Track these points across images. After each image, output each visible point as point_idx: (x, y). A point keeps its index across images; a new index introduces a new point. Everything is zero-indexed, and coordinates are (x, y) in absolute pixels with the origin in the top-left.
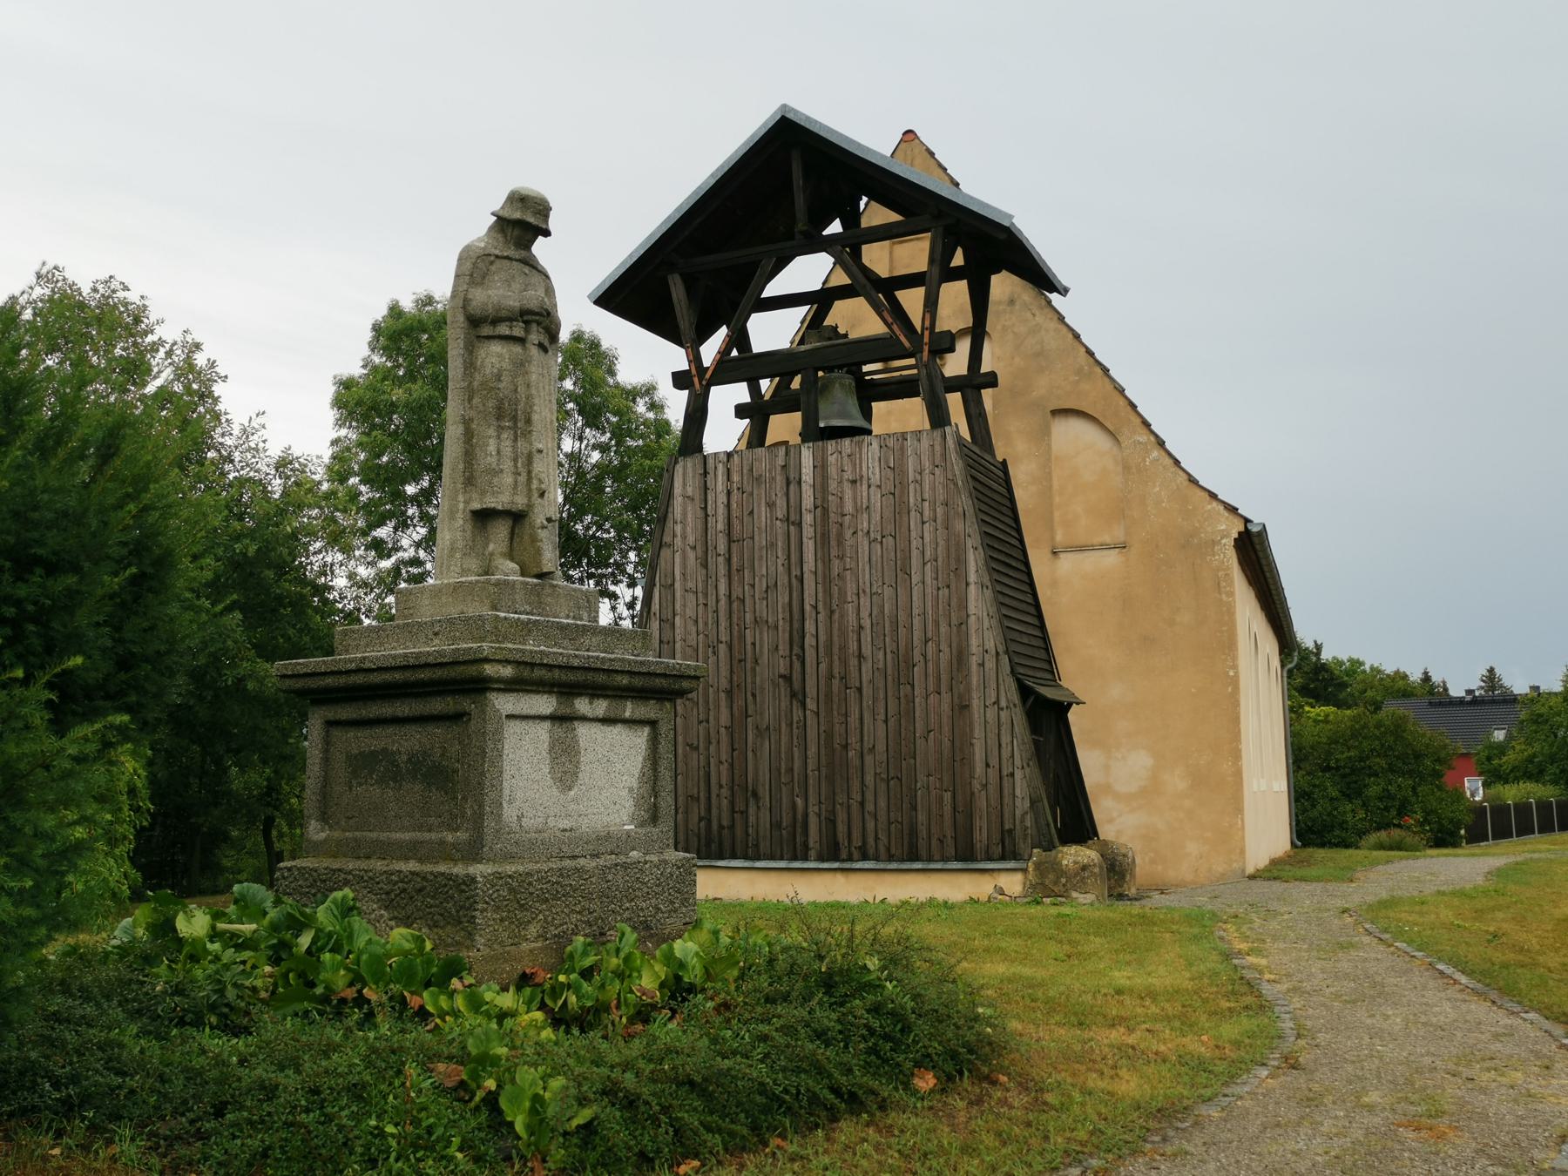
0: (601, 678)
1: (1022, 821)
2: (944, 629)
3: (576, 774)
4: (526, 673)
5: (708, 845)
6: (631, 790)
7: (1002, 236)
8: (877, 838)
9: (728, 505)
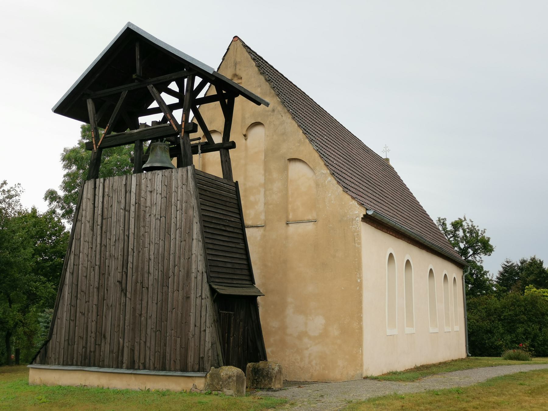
1: (208, 353)
5: (85, 360)
8: (150, 359)
9: (103, 202)
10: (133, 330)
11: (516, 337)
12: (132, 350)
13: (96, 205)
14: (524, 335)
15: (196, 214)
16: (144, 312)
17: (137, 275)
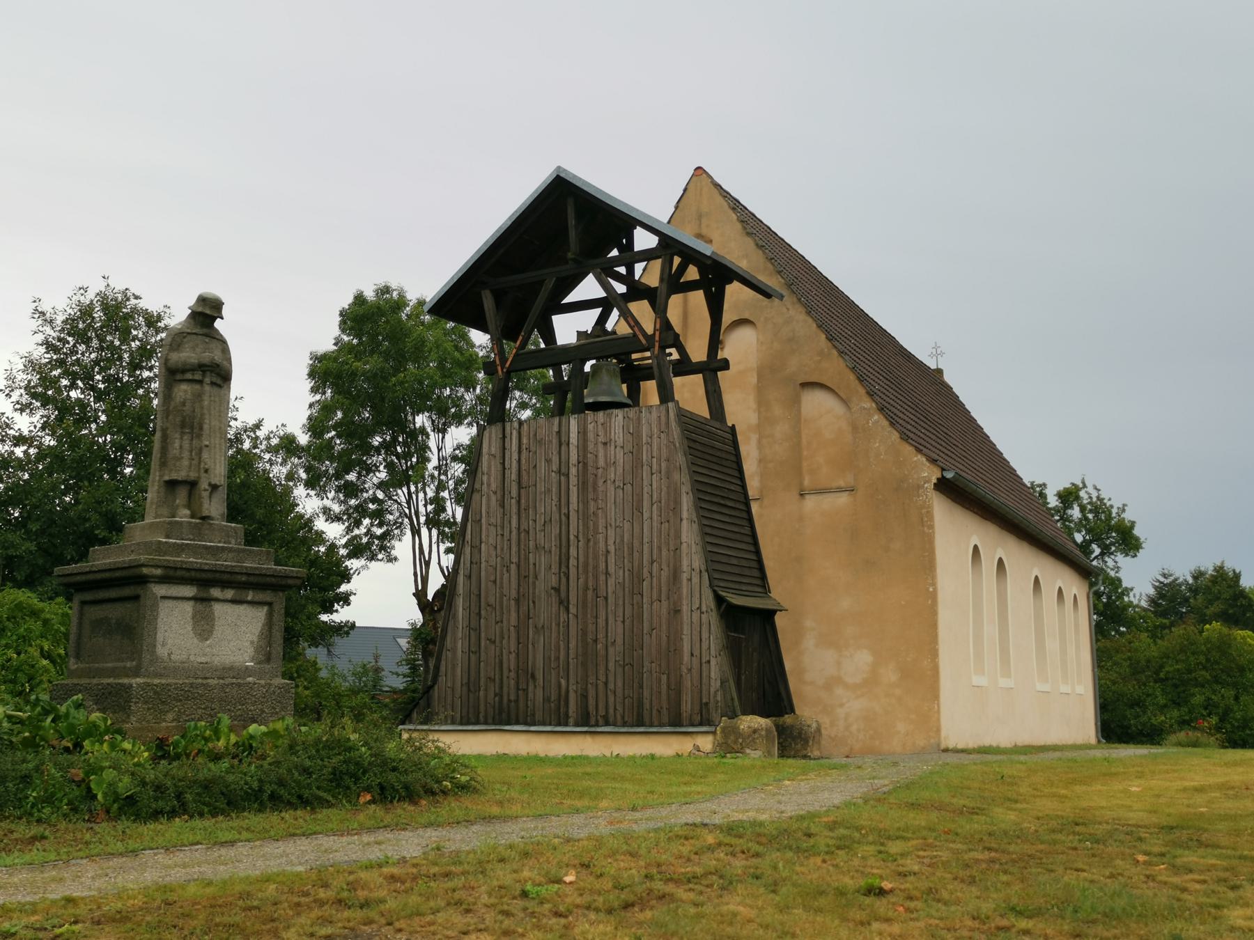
0: (226, 577)
1: (715, 696)
2: (664, 552)
3: (211, 632)
4: (171, 573)
5: (500, 714)
6: (252, 642)
7: (709, 262)
8: (615, 709)
9: (519, 461)
10: (584, 664)
11: (1190, 712)
12: (585, 697)
13: (507, 465)
14: (1206, 709)
15: (685, 478)
16: (601, 636)
17: (587, 579)
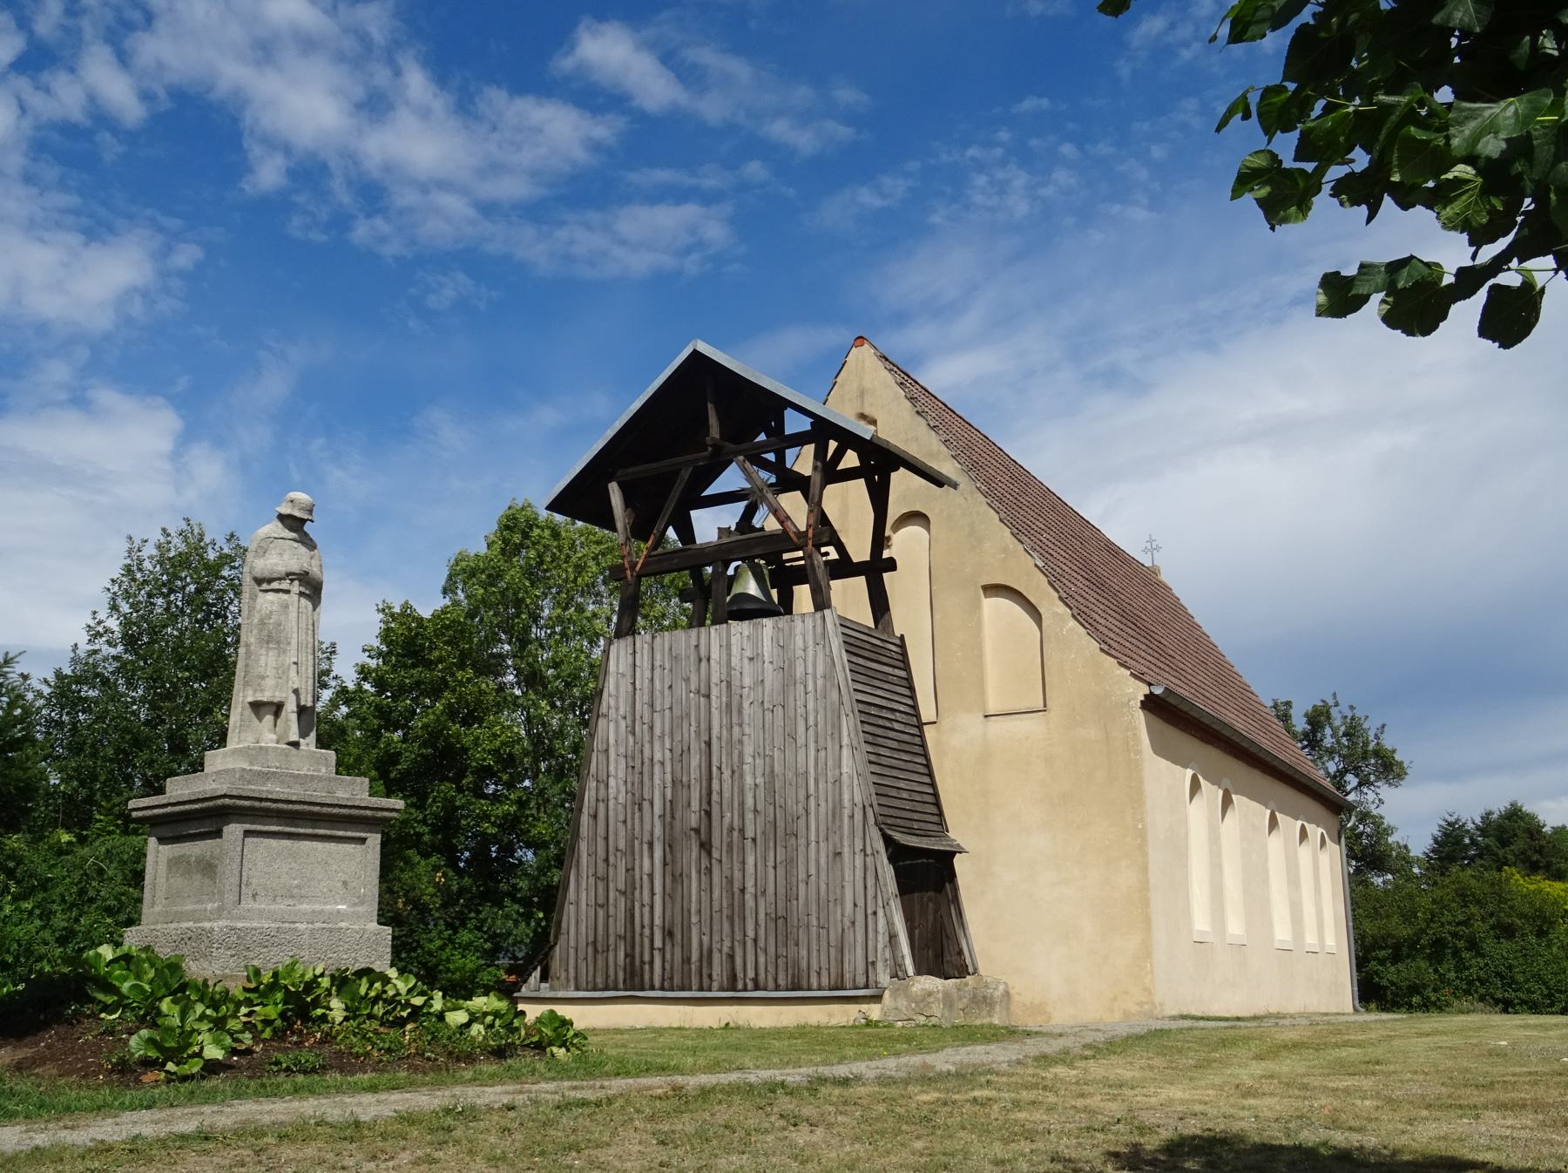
16: (750, 884)
